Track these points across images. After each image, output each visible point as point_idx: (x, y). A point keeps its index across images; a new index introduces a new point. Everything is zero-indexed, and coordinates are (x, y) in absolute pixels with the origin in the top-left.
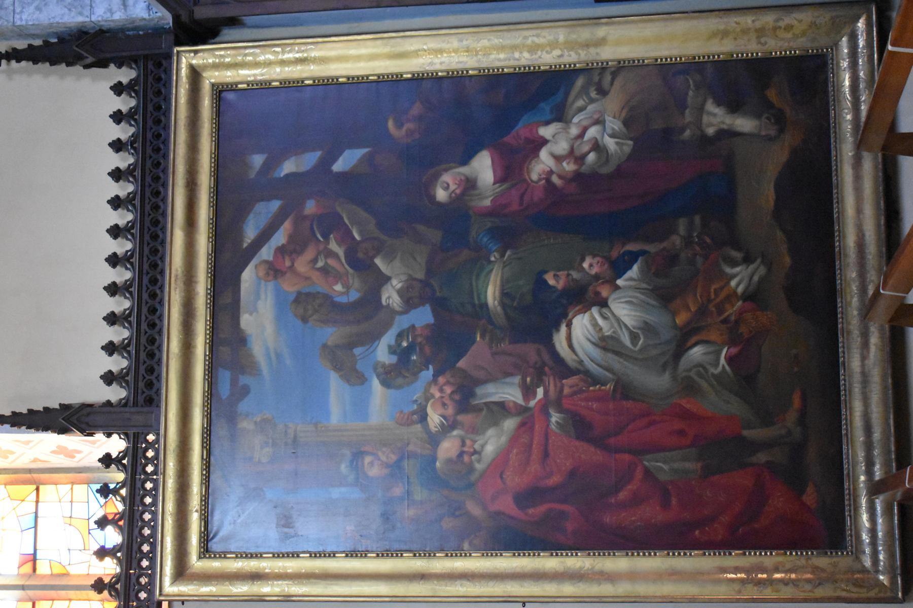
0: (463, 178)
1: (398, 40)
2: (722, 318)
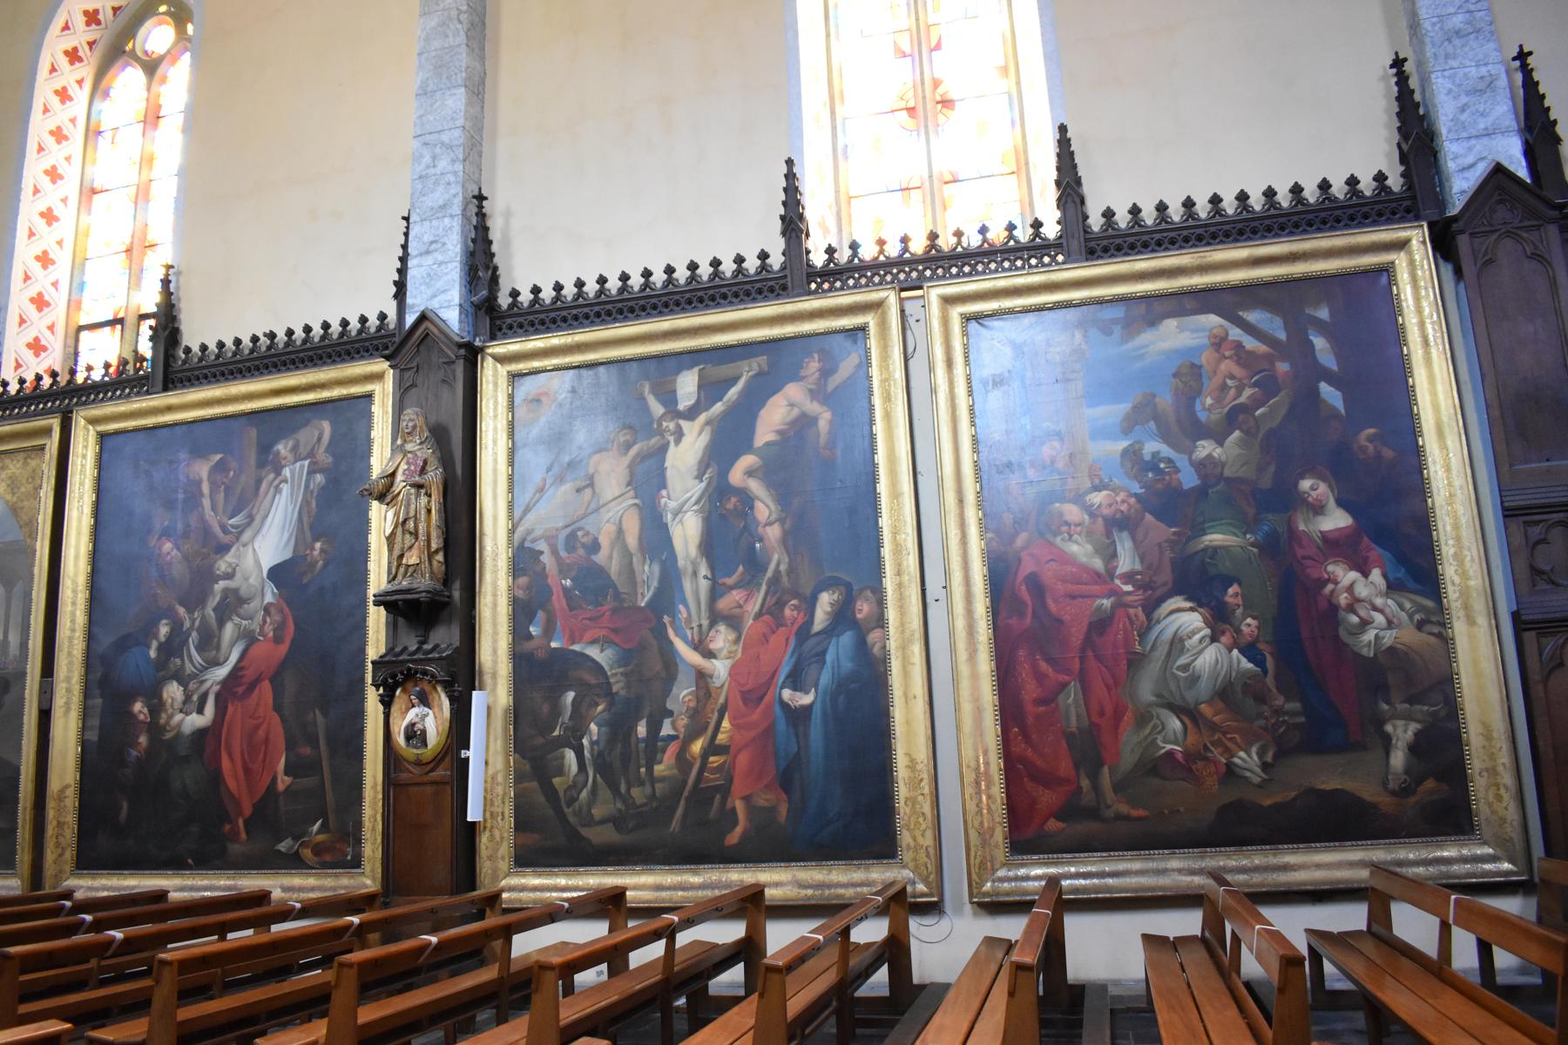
0: (1324, 502)
1: (1456, 429)
2: (1209, 745)
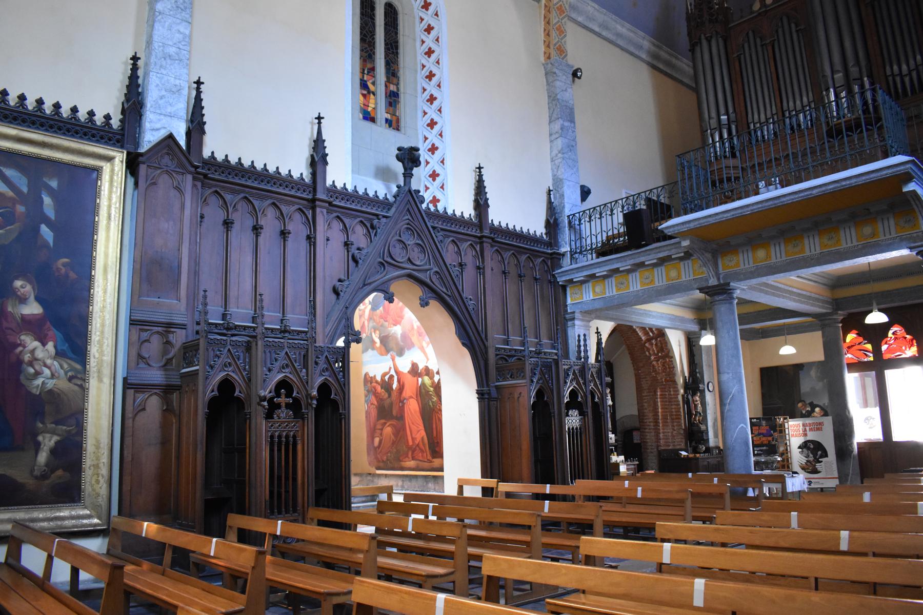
1: (114, 270)
